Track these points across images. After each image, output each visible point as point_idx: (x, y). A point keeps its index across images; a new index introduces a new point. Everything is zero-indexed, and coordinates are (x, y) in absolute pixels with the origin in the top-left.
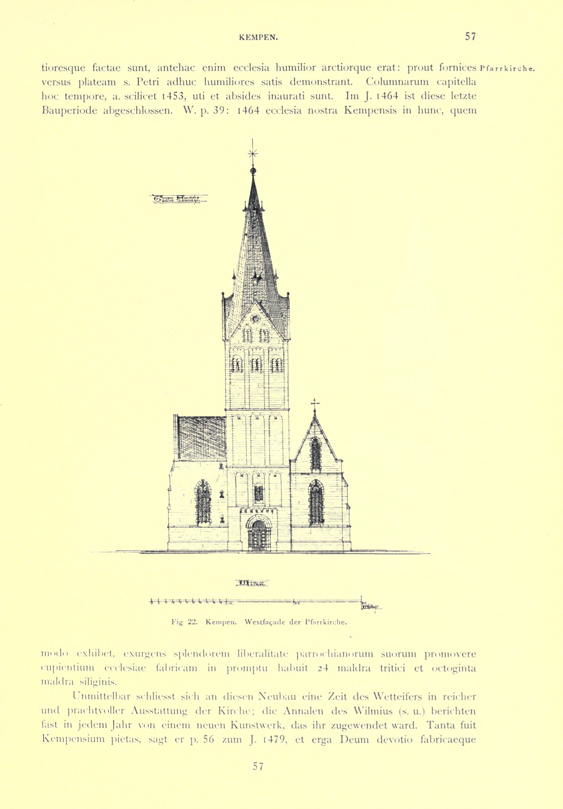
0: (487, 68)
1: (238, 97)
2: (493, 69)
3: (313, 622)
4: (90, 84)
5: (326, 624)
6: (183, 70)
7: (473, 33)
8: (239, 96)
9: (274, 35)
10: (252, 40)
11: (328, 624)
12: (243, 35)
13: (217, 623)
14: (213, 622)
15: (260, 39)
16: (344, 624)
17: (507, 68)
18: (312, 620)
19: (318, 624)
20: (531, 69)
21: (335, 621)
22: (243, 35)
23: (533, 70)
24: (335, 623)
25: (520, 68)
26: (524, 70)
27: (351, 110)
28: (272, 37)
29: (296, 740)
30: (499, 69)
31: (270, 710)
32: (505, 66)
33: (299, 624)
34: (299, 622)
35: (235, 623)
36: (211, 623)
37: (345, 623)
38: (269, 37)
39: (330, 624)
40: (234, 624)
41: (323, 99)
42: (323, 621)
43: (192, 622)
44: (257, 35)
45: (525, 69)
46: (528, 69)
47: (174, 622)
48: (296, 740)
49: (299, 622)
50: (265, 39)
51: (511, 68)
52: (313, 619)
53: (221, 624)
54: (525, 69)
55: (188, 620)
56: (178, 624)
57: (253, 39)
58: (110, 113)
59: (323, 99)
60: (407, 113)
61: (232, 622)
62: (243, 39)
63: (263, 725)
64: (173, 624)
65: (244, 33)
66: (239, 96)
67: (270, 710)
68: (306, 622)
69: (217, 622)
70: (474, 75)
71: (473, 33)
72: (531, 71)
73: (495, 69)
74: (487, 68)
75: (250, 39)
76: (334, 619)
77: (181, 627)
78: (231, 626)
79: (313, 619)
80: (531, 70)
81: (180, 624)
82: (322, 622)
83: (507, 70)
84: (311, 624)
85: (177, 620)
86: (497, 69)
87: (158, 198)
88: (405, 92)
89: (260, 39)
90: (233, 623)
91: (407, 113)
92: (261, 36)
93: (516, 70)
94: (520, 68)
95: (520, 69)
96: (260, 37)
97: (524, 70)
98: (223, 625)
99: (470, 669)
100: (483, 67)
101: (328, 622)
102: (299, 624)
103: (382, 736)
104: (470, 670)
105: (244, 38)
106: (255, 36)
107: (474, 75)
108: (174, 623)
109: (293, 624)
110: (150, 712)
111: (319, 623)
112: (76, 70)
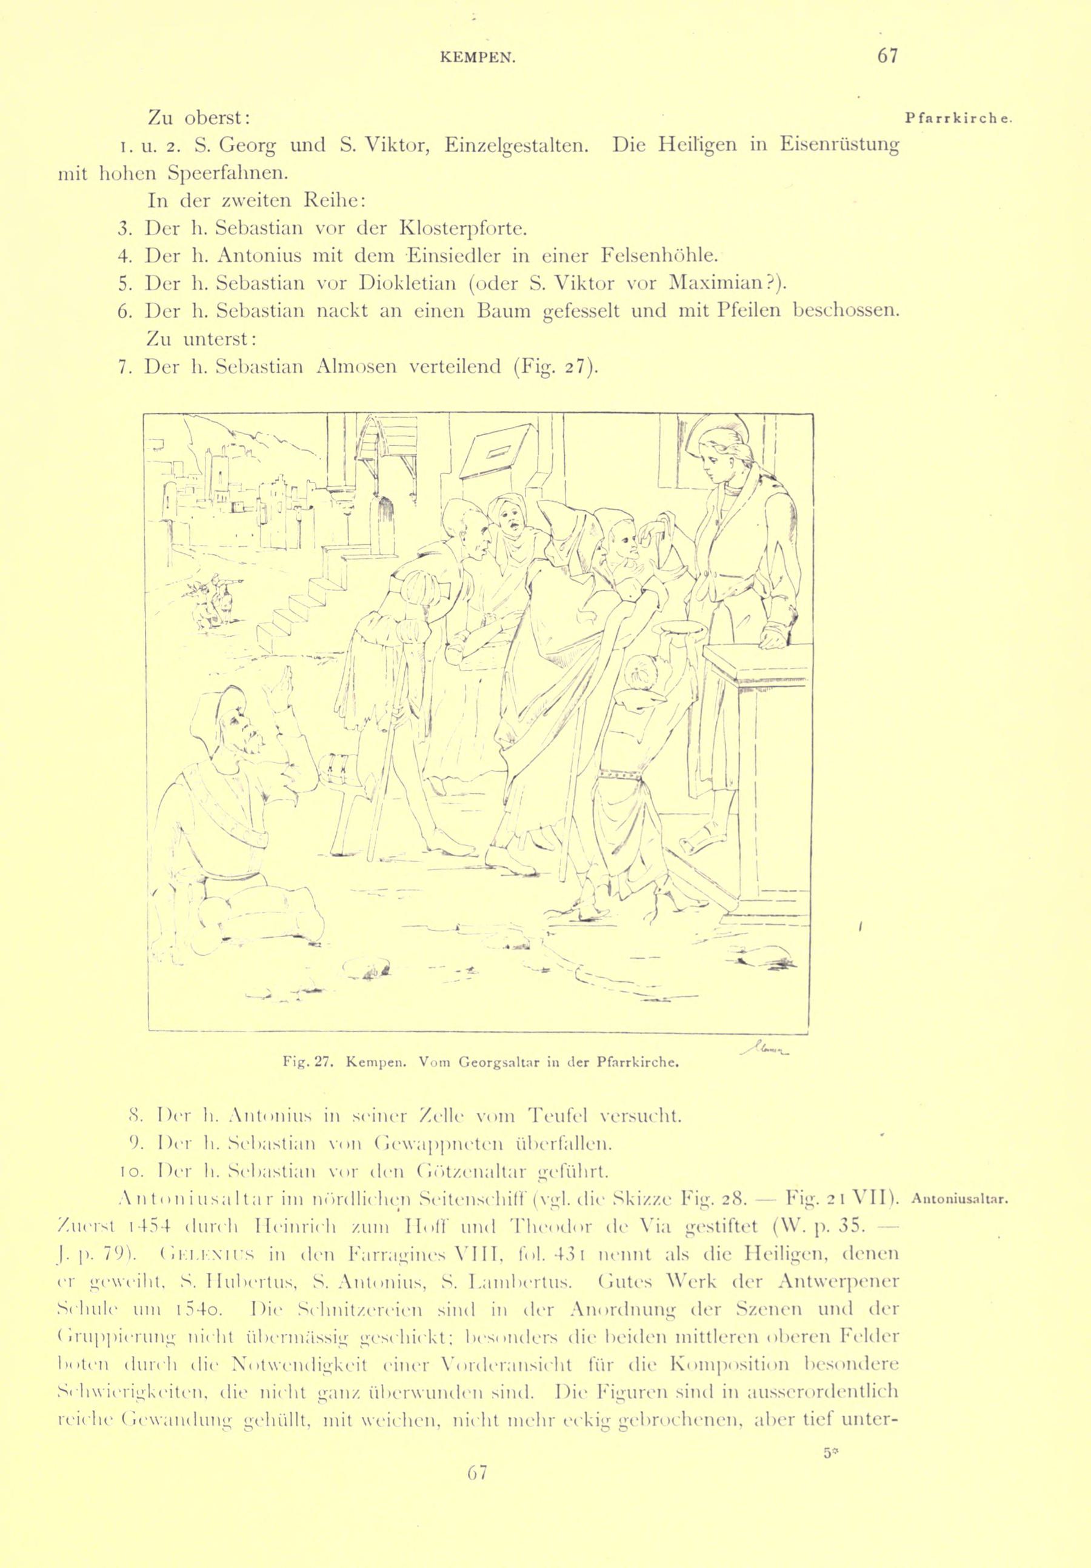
0: (921, 117)
1: (434, 230)
2: (931, 119)
3: (614, 1061)
5: (638, 1066)
6: (326, 316)
7: (892, 49)
8: (436, 229)
9: (509, 53)
10: (466, 61)
12: (448, 52)
14: (360, 1063)
15: (481, 61)
16: (673, 1066)
17: (959, 117)
18: (611, 1059)
21: (657, 1061)
22: (448, 52)
23: (1008, 120)
24: (655, 1064)
25: (985, 117)
27: (356, 1061)
28: (505, 56)
30: (942, 120)
32: (955, 113)
34: (585, 1062)
35: (402, 1065)
36: (357, 1063)
37: (675, 1064)
38: (499, 57)
40: (401, 1066)
42: (632, 1059)
43: (321, 1061)
46: (999, 120)
47: (288, 1061)
50: (491, 61)
51: (966, 117)
52: (612, 1057)
53: (376, 1065)
55: (316, 1058)
56: (295, 1065)
57: (468, 60)
61: (397, 1062)
62: (449, 61)
63: (821, 1282)
65: (451, 47)
66: (436, 229)
69: (368, 1061)
71: (892, 49)
72: (1006, 122)
73: (935, 119)
74: (921, 117)
75: (462, 61)
79: (612, 1057)
80: (1004, 120)
82: (630, 1061)
83: (959, 122)
84: (609, 1066)
85: (293, 1058)
86: (974, 119)
87: (399, 1063)
88: (697, 302)
92: (484, 55)
93: (977, 120)
94: (985, 117)
95: (983, 120)
96: (481, 57)
99: (507, 1173)
100: (911, 115)
101: (642, 1061)
103: (852, 1247)
104: (507, 1174)
105: (450, 59)
106: (471, 55)
108: (287, 1063)
109: (574, 1065)
111: (625, 1064)
112: (165, 344)
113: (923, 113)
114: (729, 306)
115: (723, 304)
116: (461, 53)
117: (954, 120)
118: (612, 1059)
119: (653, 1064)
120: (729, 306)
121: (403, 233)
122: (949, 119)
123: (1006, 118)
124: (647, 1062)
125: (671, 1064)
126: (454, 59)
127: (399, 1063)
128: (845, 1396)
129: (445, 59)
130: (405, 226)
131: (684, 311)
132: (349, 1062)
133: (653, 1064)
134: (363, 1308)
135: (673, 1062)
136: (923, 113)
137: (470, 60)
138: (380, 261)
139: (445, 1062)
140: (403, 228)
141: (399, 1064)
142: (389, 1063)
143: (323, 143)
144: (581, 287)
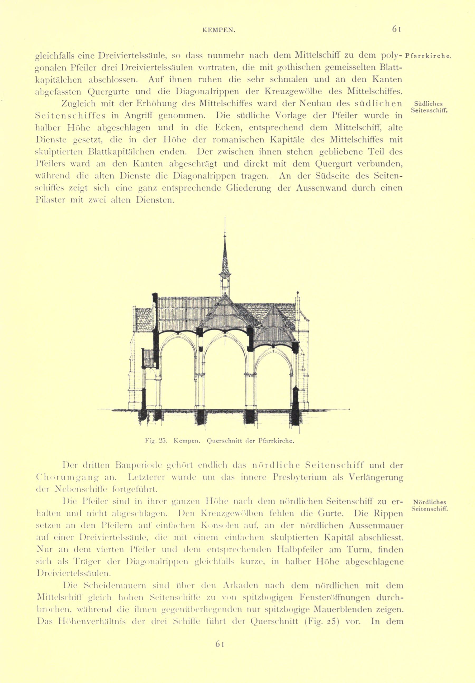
0: (412, 55)
2: (416, 57)
4: (390, 69)
5: (276, 442)
10: (213, 32)
11: (278, 442)
13: (183, 442)
14: (180, 441)
17: (428, 55)
19: (269, 442)
20: (449, 56)
23: (450, 57)
24: (284, 441)
25: (439, 55)
26: (442, 57)
27: (178, 440)
29: (161, 152)
30: (421, 57)
31: (162, 175)
33: (220, 442)
34: (253, 440)
36: (178, 441)
37: (292, 442)
38: (228, 30)
39: (280, 442)
41: (320, 81)
42: (274, 440)
43: (162, 440)
44: (217, 28)
45: (443, 56)
48: (161, 152)
49: (253, 440)
50: (224, 32)
51: (431, 55)
52: (265, 438)
54: (443, 56)
57: (214, 31)
58: (95, 82)
59: (320, 81)
60: (86, 58)
64: (146, 442)
67: (162, 175)
68: (260, 441)
69: (183, 440)
70: (400, 61)
73: (418, 56)
74: (412, 55)
75: (227, 32)
76: (283, 438)
77: (153, 444)
78: (195, 444)
79: (265, 438)
80: (448, 57)
81: (152, 443)
83: (428, 57)
84: (264, 442)
85: (150, 439)
86: (435, 56)
87: (197, 441)
89: (220, 31)
90: (197, 441)
91: (86, 58)
92: (221, 29)
94: (439, 55)
97: (442, 57)
98: (189, 444)
100: (408, 55)
102: (220, 442)
106: (216, 29)
107: (400, 61)
110: (126, 538)
111: (271, 442)
113: (413, 54)
114: (75, 66)
115: (73, 65)
116: (211, 28)
117: (426, 57)
118: (265, 440)
119: (283, 441)
120: (75, 66)
121: (272, 142)
122: (424, 56)
123: (449, 56)
124: (280, 441)
125: (291, 442)
126: (208, 31)
127: (197, 441)
128: (137, 588)
129: (204, 31)
130: (272, 138)
131: (262, 68)
132: (175, 441)
133: (283, 441)
134: (224, 512)
135: (292, 441)
136: (413, 54)
137: (215, 31)
138: (304, 166)
139: (185, 441)
140: (272, 140)
141: (197, 441)
142: (192, 441)
143: (302, 126)
144: (228, 129)
